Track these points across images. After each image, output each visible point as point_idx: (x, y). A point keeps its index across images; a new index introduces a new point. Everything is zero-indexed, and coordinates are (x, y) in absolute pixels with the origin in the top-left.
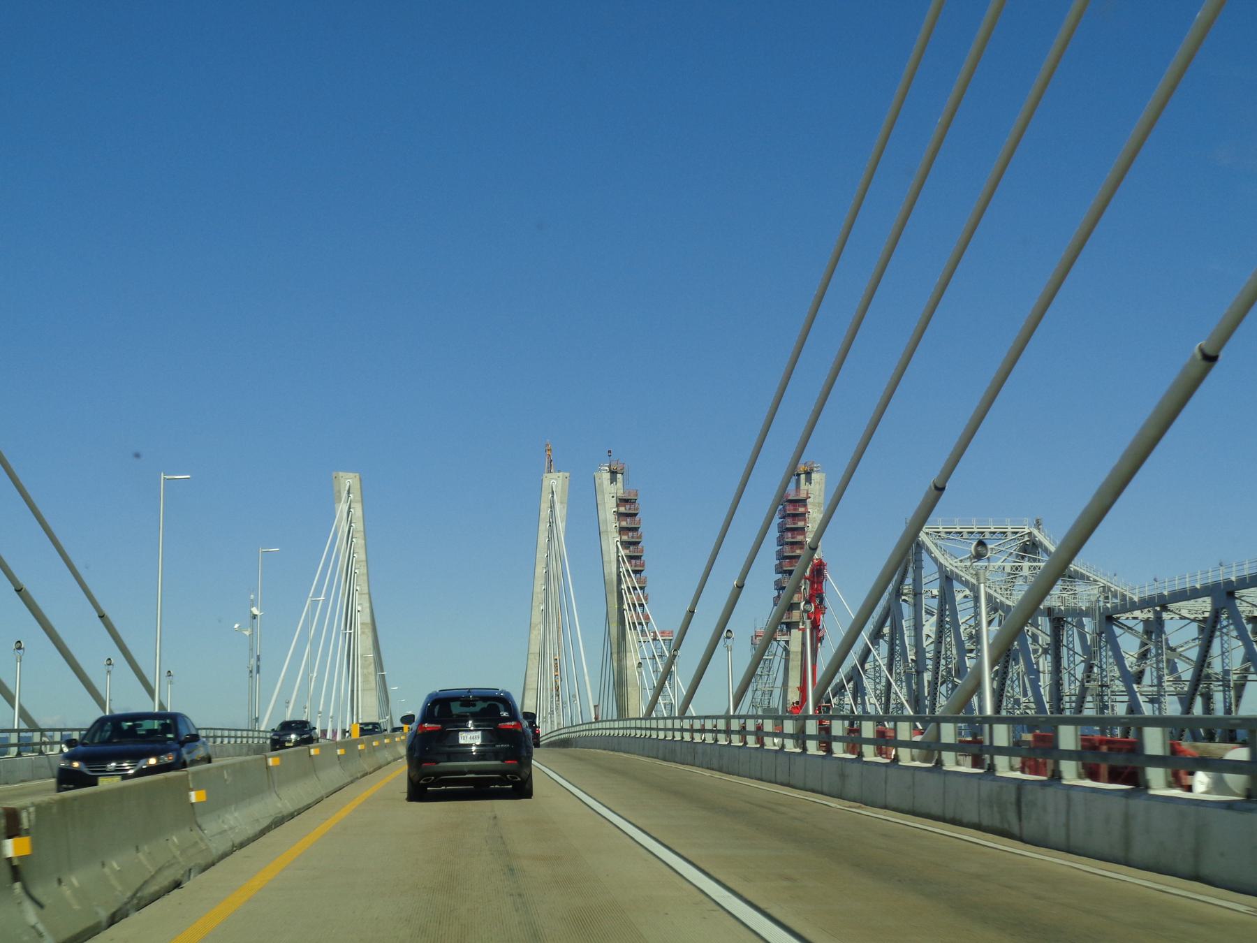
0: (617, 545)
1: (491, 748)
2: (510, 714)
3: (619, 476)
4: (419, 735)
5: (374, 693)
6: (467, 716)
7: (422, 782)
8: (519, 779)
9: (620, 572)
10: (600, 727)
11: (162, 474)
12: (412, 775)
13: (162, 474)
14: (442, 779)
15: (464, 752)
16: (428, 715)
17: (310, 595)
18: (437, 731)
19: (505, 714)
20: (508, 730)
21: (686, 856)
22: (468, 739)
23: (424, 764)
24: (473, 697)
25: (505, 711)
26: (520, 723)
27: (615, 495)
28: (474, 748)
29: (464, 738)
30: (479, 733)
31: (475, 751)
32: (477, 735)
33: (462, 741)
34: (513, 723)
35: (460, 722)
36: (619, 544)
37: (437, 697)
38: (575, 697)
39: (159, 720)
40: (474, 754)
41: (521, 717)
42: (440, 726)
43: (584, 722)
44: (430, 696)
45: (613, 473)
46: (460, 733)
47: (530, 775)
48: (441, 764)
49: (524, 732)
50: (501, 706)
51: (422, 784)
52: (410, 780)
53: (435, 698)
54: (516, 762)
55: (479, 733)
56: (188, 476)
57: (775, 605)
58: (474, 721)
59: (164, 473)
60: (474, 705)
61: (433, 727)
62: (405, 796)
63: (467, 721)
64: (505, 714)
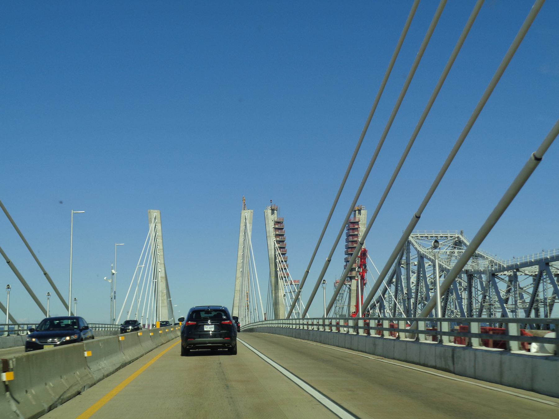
0: (274, 242)
1: (218, 332)
2: (227, 317)
3: (275, 211)
4: (186, 326)
5: (166, 308)
6: (208, 318)
7: (188, 347)
8: (231, 346)
9: (276, 254)
10: (267, 323)
11: (72, 211)
12: (183, 344)
13: (72, 211)
14: (197, 346)
15: (206, 334)
16: (190, 318)
17: (138, 264)
18: (194, 325)
19: (224, 317)
20: (226, 325)
21: (305, 380)
22: (208, 329)
23: (189, 340)
24: (210, 310)
25: (225, 316)
26: (231, 321)
27: (273, 220)
28: (211, 333)
29: (207, 328)
30: (213, 326)
31: (211, 334)
32: (212, 326)
33: (205, 329)
34: (228, 321)
35: (205, 321)
36: (275, 242)
37: (194, 310)
38: (256, 310)
39: (71, 320)
40: (211, 335)
41: (232, 318)
42: (195, 322)
43: (260, 321)
44: (191, 309)
45: (273, 210)
46: (205, 326)
47: (236, 345)
48: (196, 339)
49: (233, 325)
50: (223, 314)
51: (188, 348)
52: (182, 346)
53: (193, 310)
54: (229, 339)
55: (213, 326)
56: (84, 212)
57: (345, 269)
58: (211, 320)
59: (73, 210)
60: (211, 313)
61: (192, 323)
62: (180, 353)
63: (208, 320)
64: (224, 317)
